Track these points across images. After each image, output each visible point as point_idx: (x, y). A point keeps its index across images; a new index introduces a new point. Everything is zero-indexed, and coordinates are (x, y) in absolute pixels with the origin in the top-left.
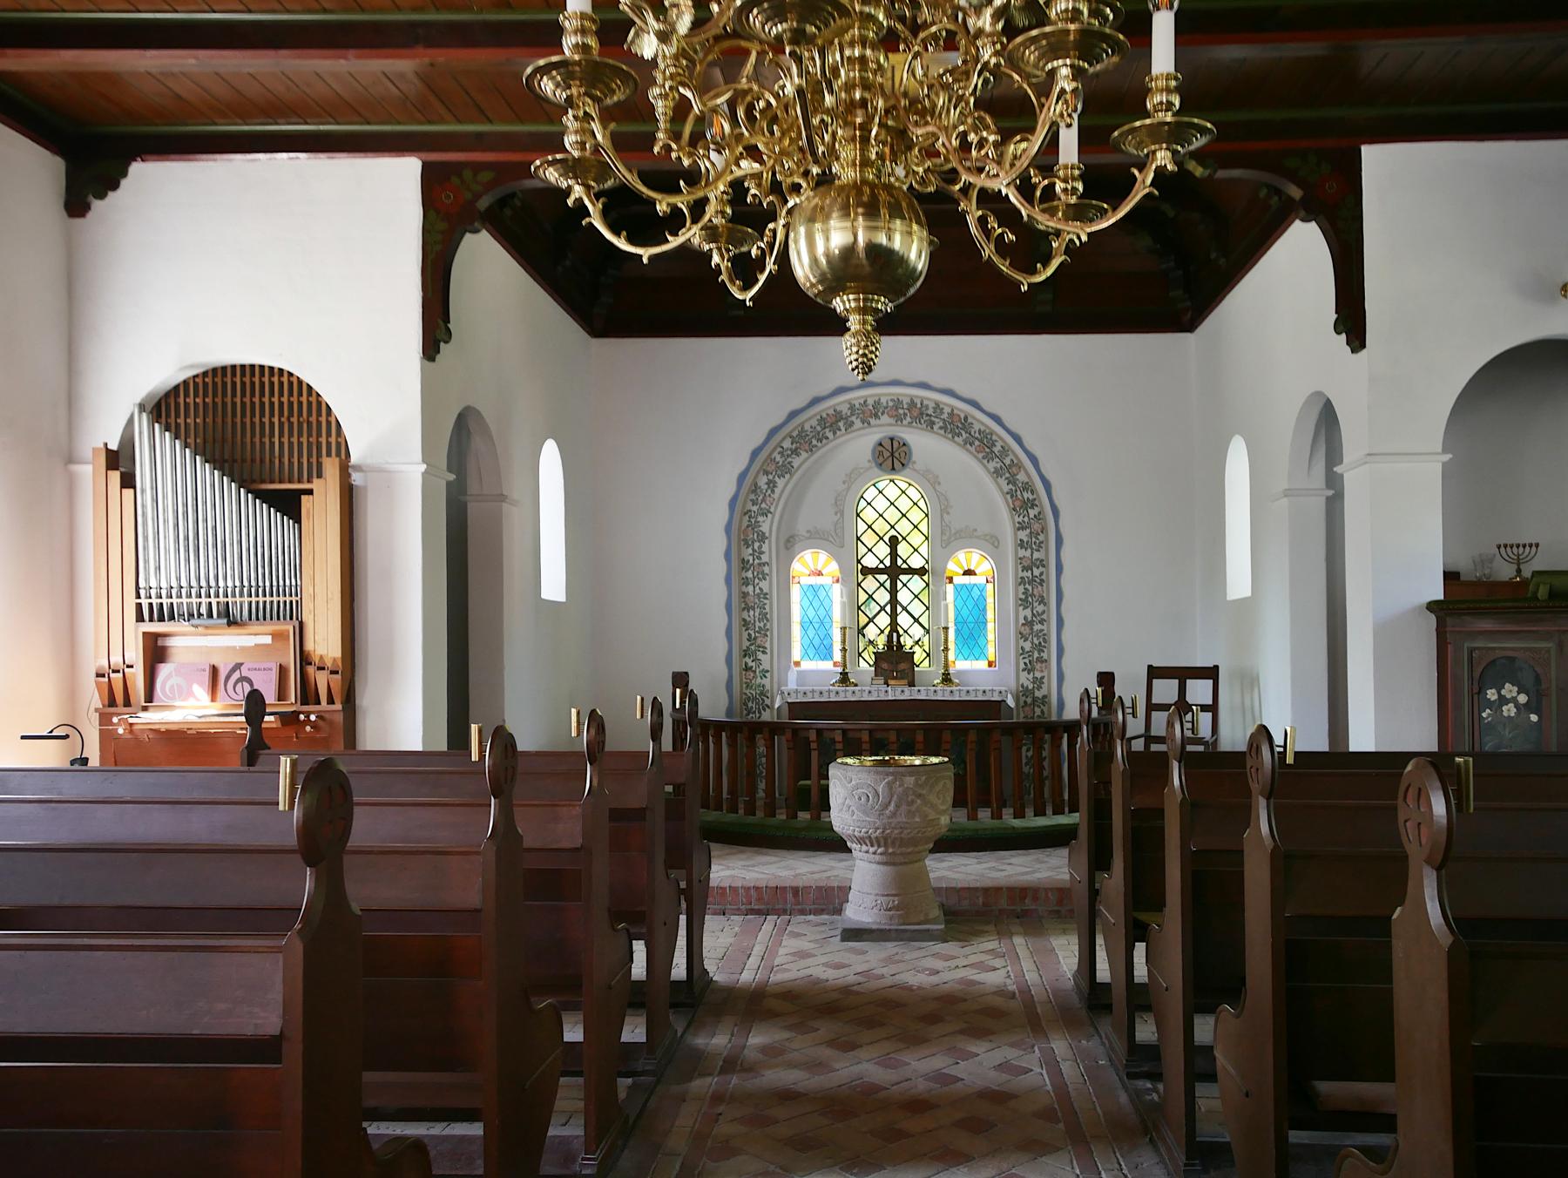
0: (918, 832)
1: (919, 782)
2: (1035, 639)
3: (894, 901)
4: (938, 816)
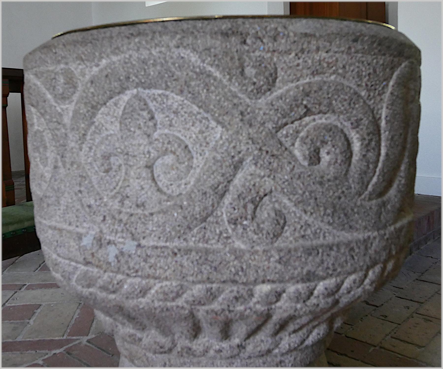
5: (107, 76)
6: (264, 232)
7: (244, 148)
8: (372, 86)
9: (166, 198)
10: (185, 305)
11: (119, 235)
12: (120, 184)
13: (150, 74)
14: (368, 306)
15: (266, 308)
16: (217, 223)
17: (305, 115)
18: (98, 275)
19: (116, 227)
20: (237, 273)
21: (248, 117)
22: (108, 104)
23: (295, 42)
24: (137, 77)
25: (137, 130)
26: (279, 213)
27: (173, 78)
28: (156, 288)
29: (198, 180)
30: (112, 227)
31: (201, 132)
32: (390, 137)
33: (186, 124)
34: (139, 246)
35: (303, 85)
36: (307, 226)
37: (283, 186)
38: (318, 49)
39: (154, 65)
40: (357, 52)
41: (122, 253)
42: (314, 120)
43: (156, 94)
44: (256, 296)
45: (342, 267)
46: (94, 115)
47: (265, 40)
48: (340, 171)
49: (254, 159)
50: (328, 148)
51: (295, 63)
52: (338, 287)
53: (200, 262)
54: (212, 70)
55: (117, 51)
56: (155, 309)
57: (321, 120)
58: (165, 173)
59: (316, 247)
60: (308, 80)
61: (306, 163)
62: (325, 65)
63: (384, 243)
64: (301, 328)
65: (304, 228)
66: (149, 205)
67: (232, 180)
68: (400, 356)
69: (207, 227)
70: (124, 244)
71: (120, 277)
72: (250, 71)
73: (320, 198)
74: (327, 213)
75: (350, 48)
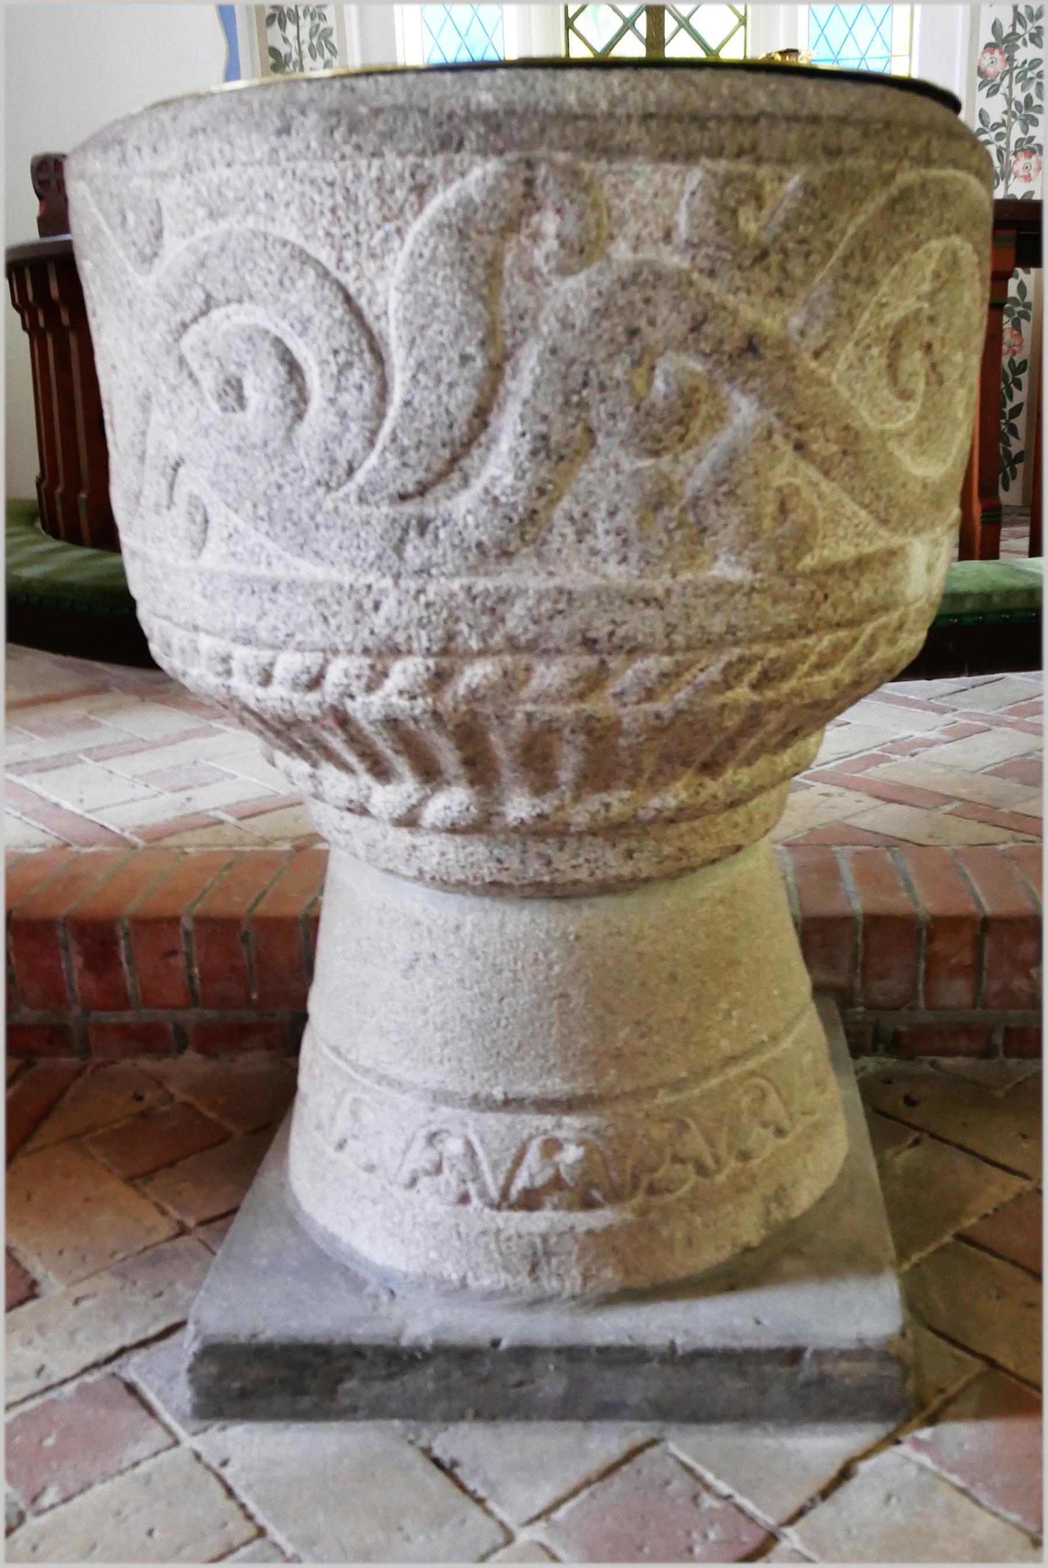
0: (728, 680)
1: (749, 223)
2: (1017, 88)
3: (552, 1147)
4: (884, 539)
75: (275, 151)
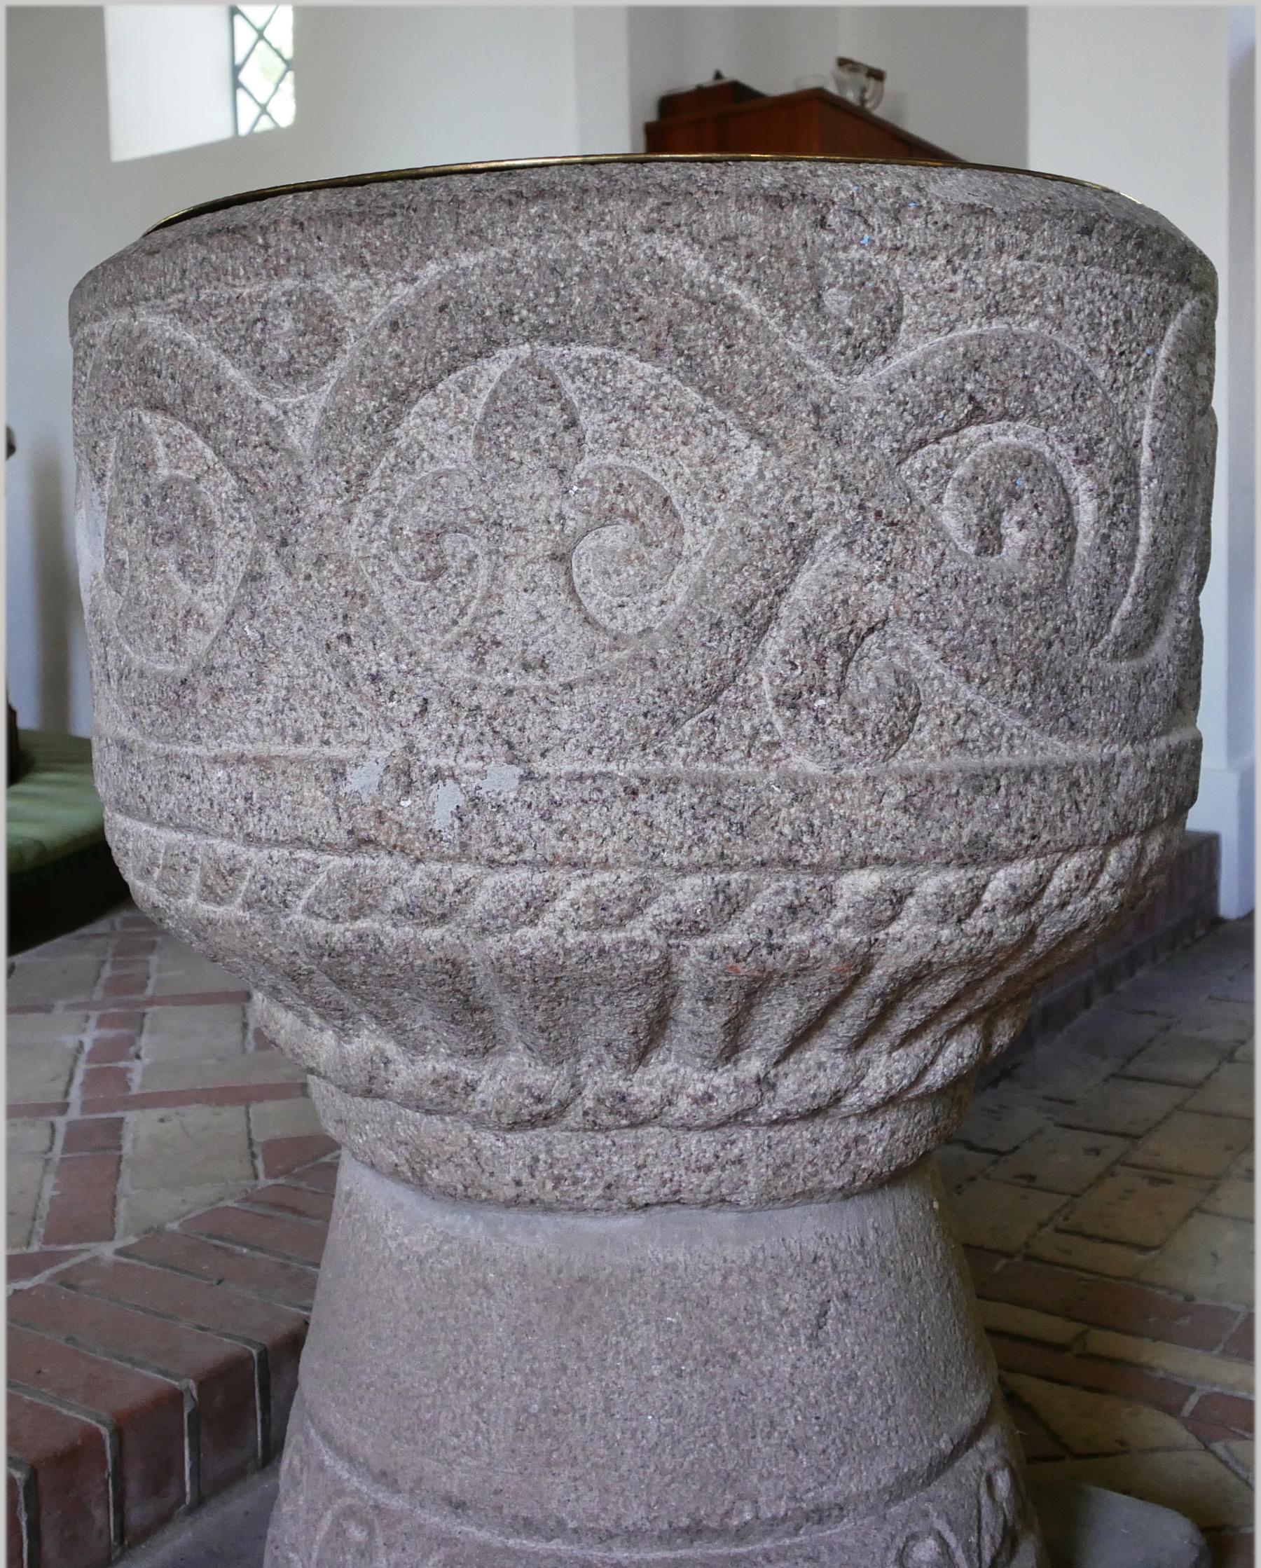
5: (442, 309)
6: (869, 728)
7: (819, 502)
8: (1122, 354)
9: (607, 641)
10: (653, 936)
11: (467, 751)
12: (471, 610)
13: (571, 303)
14: (972, 1153)
15: (865, 938)
16: (745, 706)
17: (970, 420)
18: (394, 874)
19: (461, 728)
20: (797, 840)
21: (831, 419)
22: (440, 386)
23: (946, 226)
24: (534, 309)
25: (528, 458)
26: (902, 678)
27: (637, 315)
28: (570, 895)
29: (700, 590)
30: (447, 730)
31: (707, 460)
32: (1161, 495)
33: (667, 438)
34: (528, 776)
35: (966, 341)
36: (971, 716)
37: (917, 606)
38: (1000, 248)
39: (584, 279)
40: (1089, 262)
41: (476, 802)
42: (989, 435)
43: (585, 357)
44: (842, 903)
45: (1053, 830)
46: (396, 418)
47: (873, 221)
48: (1049, 573)
49: (844, 532)
50: (1022, 509)
51: (946, 284)
52: (1042, 883)
53: (701, 811)
54: (742, 293)
55: (474, 238)
56: (568, 952)
57: (1006, 436)
58: (606, 572)
59: (994, 771)
60: (974, 329)
61: (970, 548)
62: (1017, 291)
63: (1146, 782)
64: (924, 1026)
65: (962, 721)
66: (559, 661)
67: (786, 590)
68: (1085, 1275)
69: (718, 716)
70: (483, 774)
71: (464, 871)
72: (836, 300)
73: (1004, 641)
74: (1020, 683)
75: (1073, 250)
